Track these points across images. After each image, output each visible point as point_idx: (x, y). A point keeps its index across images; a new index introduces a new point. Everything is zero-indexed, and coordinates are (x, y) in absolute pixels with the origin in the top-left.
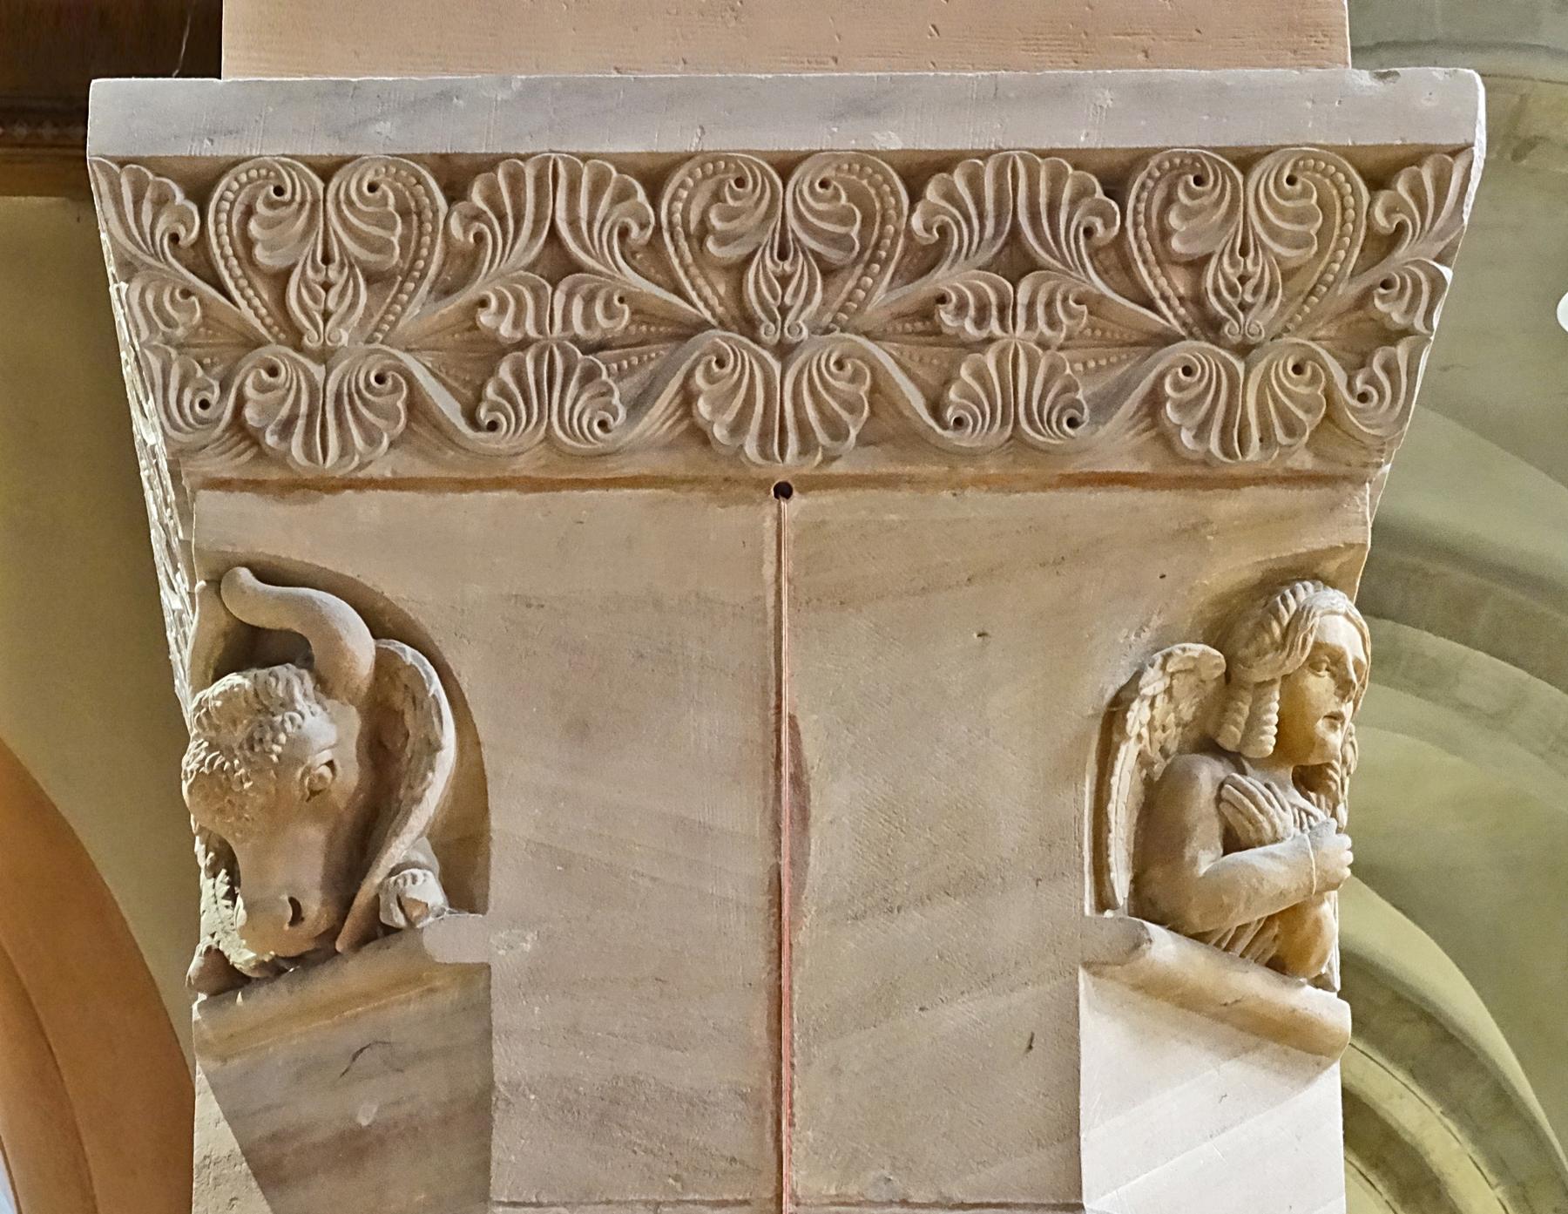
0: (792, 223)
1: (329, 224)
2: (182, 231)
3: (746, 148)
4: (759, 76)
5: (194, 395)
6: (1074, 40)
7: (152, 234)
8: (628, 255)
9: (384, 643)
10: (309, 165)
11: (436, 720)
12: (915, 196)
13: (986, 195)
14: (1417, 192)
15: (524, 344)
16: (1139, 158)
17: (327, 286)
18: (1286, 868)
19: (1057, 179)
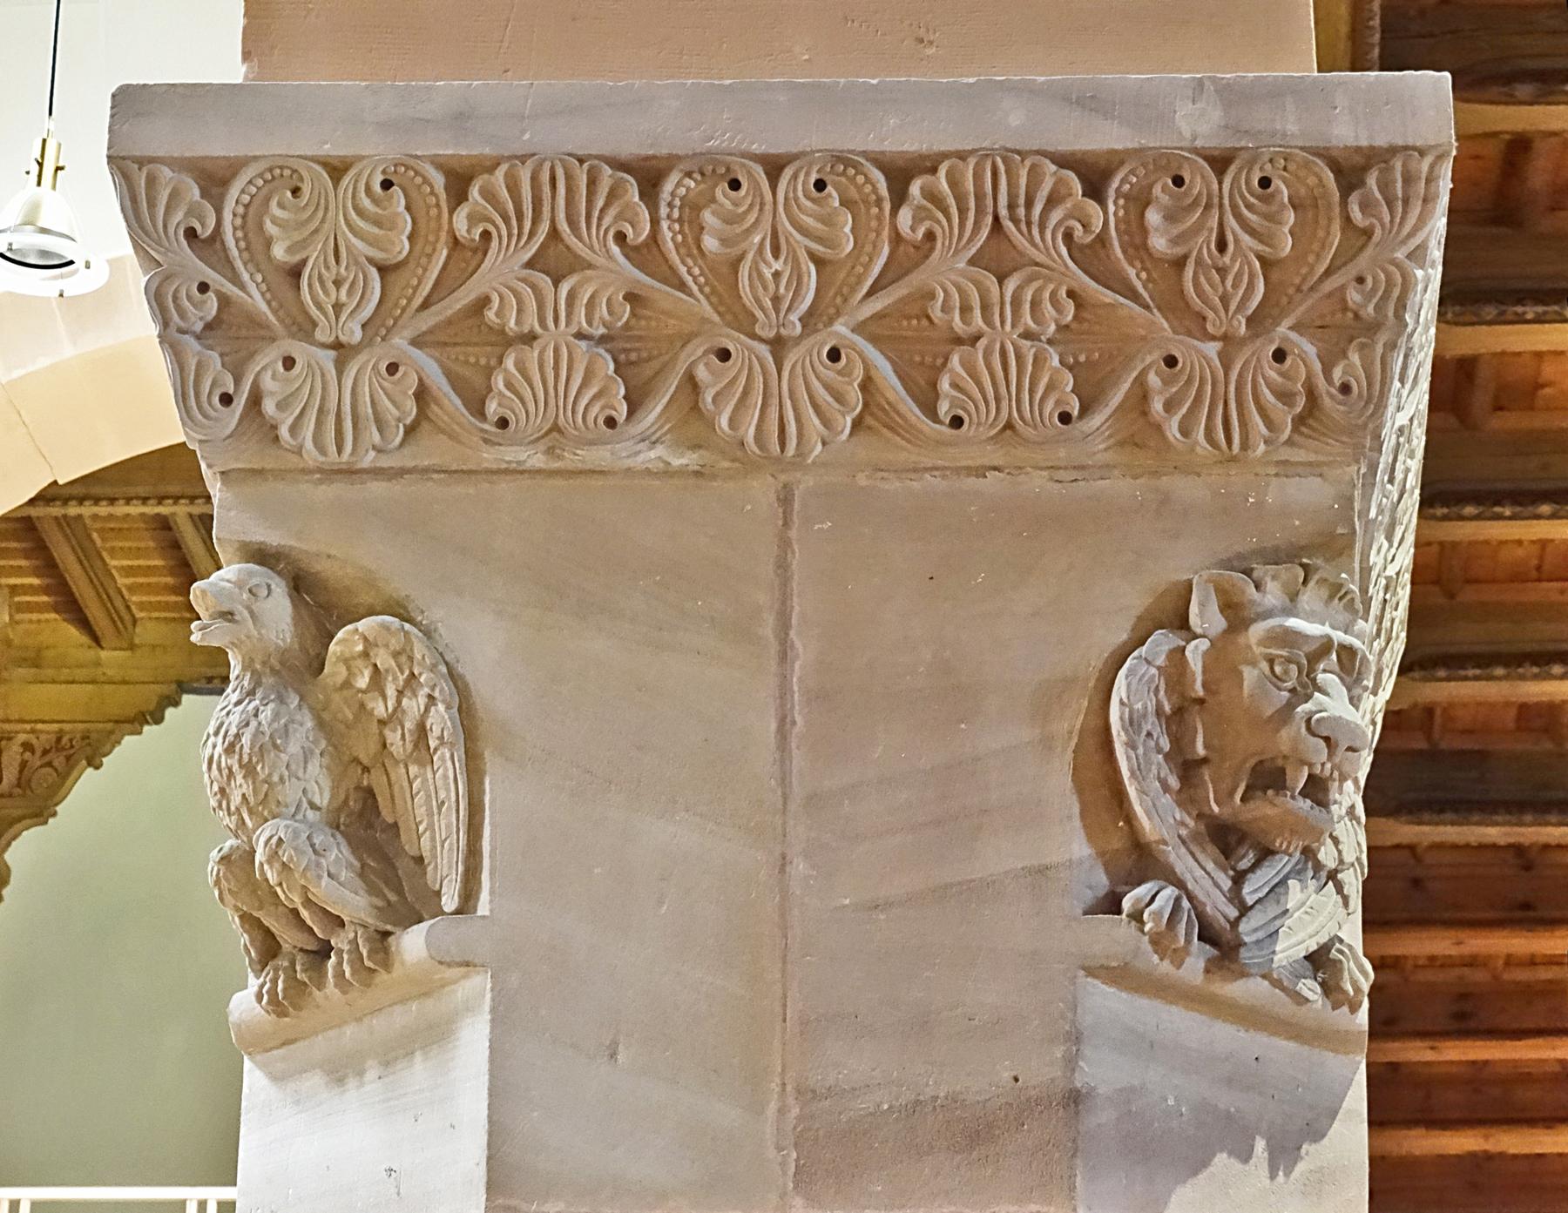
0: (1231, 221)
1: (1225, 224)
2: (629, 231)
3: (302, 153)
4: (965, 80)
5: (603, 408)
6: (371, 74)
7: (165, 226)
8: (1077, 255)
9: (355, 690)
10: (1206, 158)
11: (1545, 974)
12: (899, 197)
13: (524, 195)
14: (1385, 187)
15: (530, 338)
16: (234, 166)
17: (337, 284)
18: (1071, 1000)
19: (1034, 172)
